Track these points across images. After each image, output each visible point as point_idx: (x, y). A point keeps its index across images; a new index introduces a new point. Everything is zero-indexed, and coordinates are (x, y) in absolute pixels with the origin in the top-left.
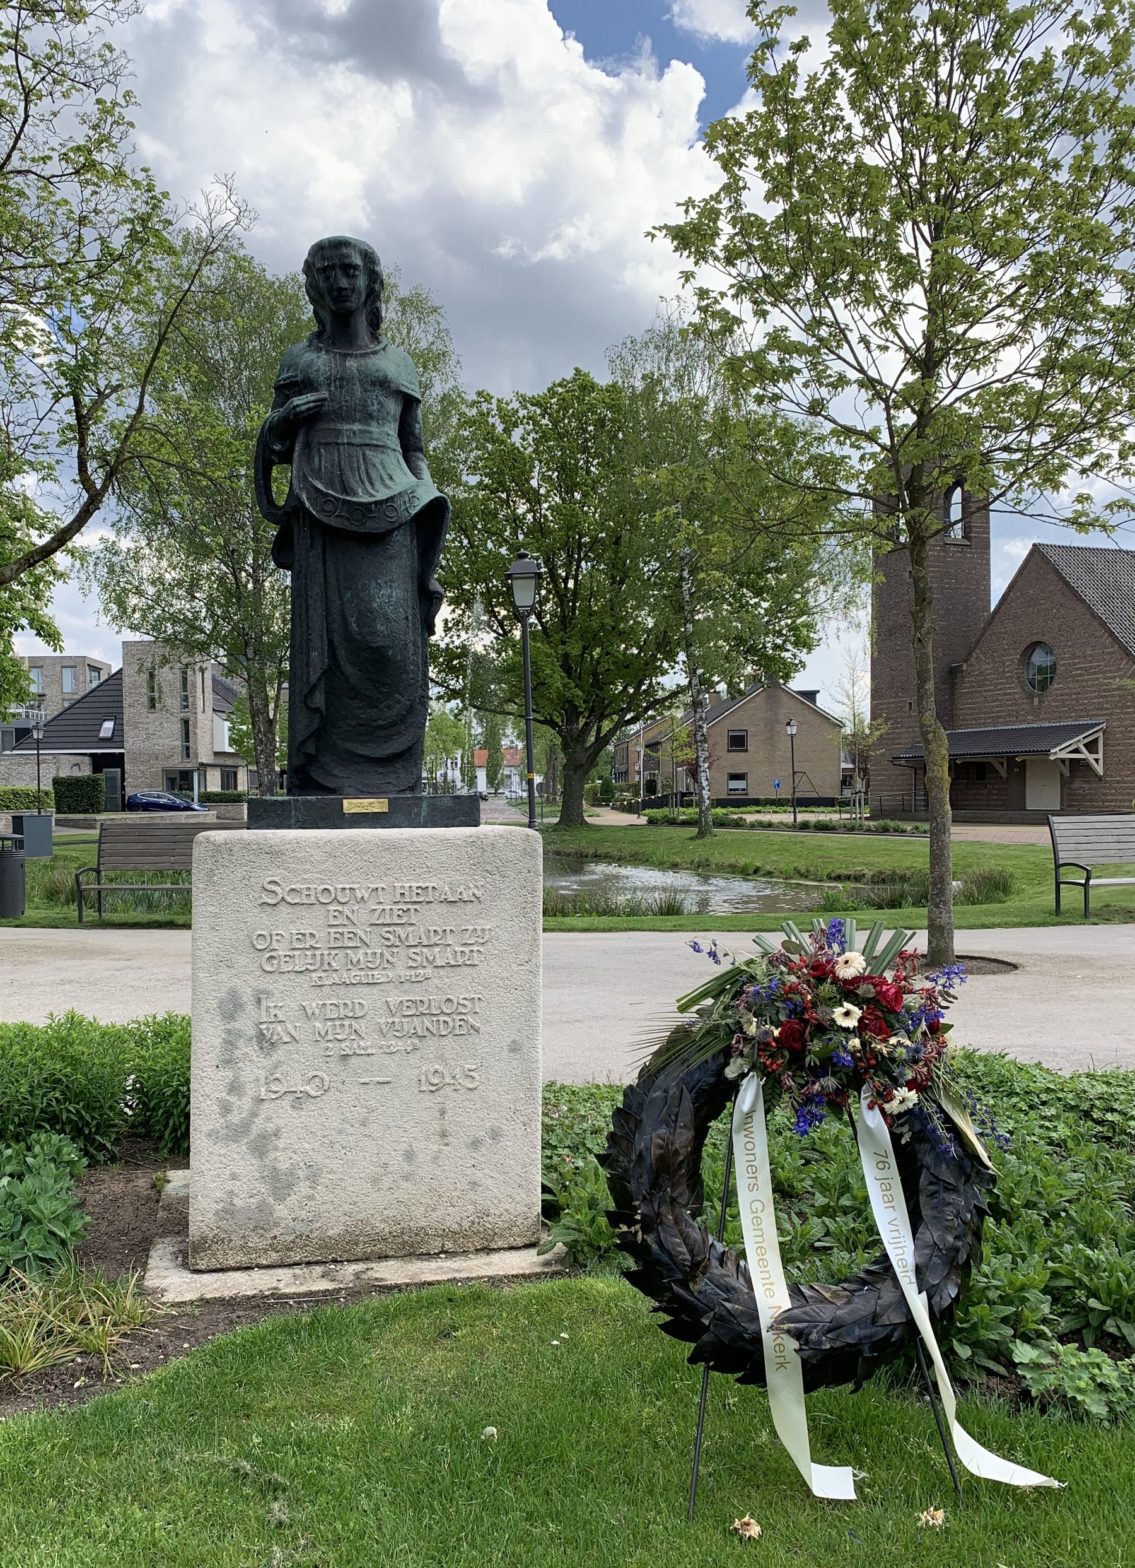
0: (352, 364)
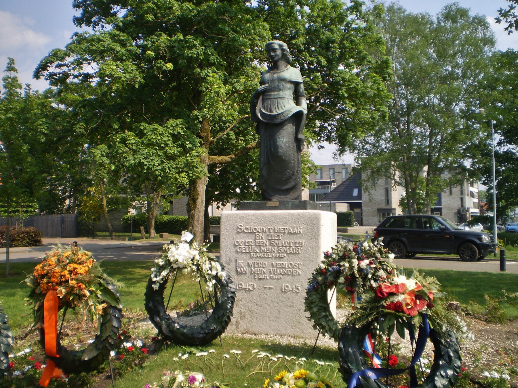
0: (276, 76)
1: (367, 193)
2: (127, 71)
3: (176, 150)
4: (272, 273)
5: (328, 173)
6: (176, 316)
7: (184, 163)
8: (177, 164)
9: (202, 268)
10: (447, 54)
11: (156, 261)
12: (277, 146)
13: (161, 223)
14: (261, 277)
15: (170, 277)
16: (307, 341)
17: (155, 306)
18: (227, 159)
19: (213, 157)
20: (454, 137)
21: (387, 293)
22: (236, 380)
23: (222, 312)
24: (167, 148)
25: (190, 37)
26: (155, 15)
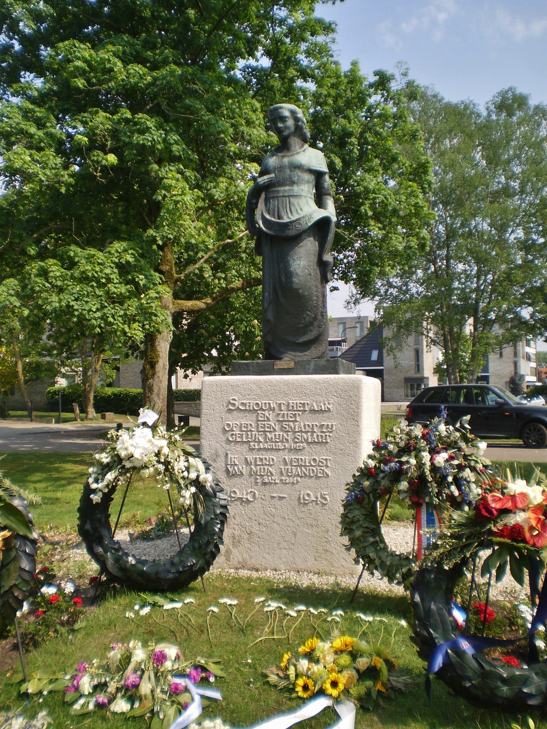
0: (286, 160)
1: (392, 356)
2: (47, 165)
3: (123, 289)
4: (285, 474)
5: (336, 329)
6: (128, 539)
7: (137, 308)
8: (126, 310)
9: (173, 468)
10: (499, 160)
11: (97, 456)
12: (291, 272)
13: (103, 398)
14: (267, 481)
15: (119, 483)
16: (339, 579)
17: (95, 529)
18: (199, 304)
19: (179, 301)
20: (508, 277)
21: (497, 510)
22: (232, 652)
23: (205, 539)
24: (110, 285)
25: (140, 115)
26: (88, 81)
